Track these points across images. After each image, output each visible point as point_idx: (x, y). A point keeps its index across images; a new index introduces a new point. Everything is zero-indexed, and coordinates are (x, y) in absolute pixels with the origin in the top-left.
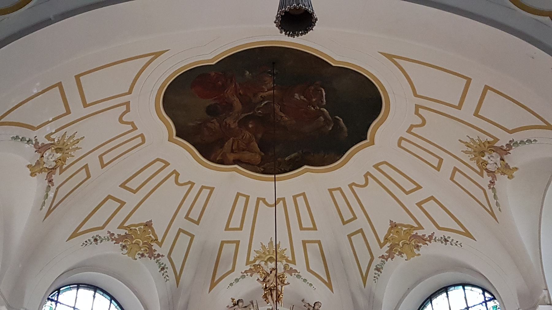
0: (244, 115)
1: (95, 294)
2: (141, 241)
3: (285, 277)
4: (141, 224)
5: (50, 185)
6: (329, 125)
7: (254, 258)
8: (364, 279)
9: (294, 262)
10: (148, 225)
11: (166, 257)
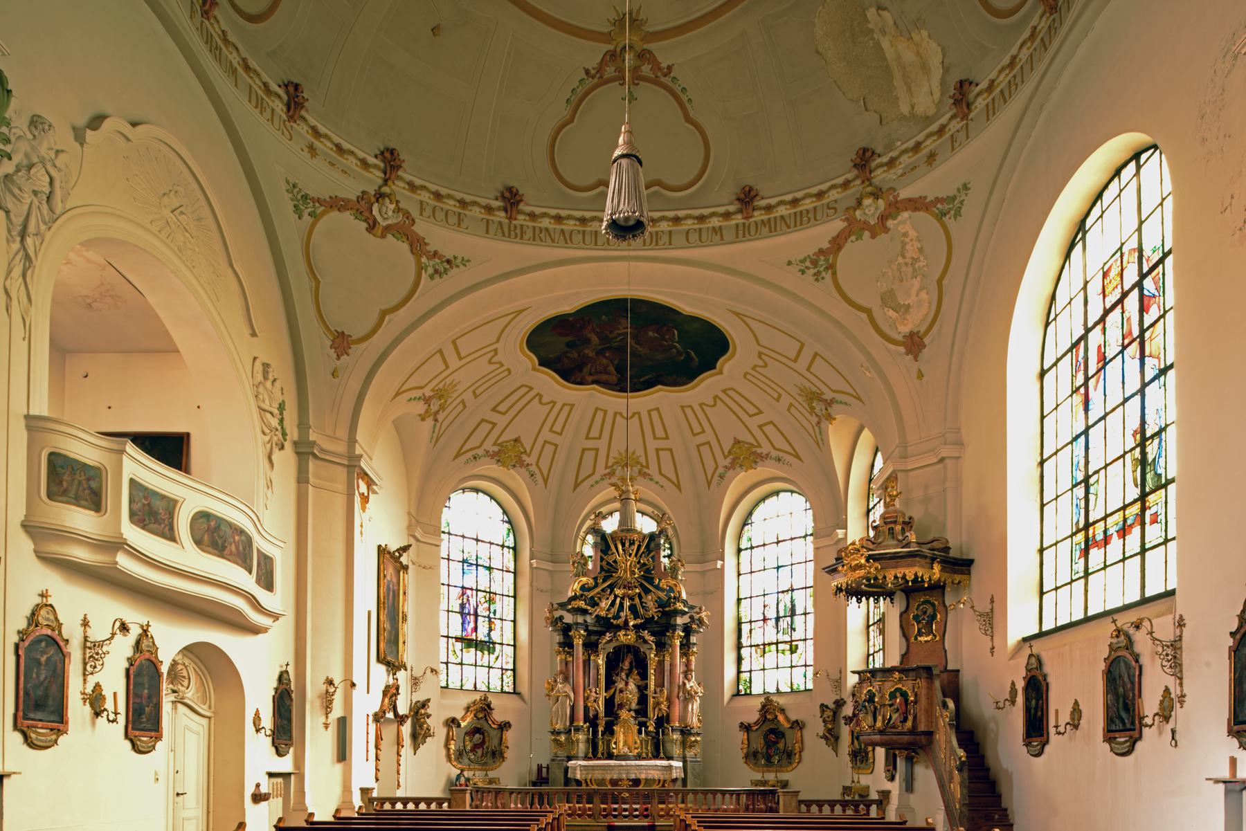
0: (601, 347)
4: (511, 440)
6: (681, 356)
8: (709, 483)
9: (647, 467)
10: (517, 440)
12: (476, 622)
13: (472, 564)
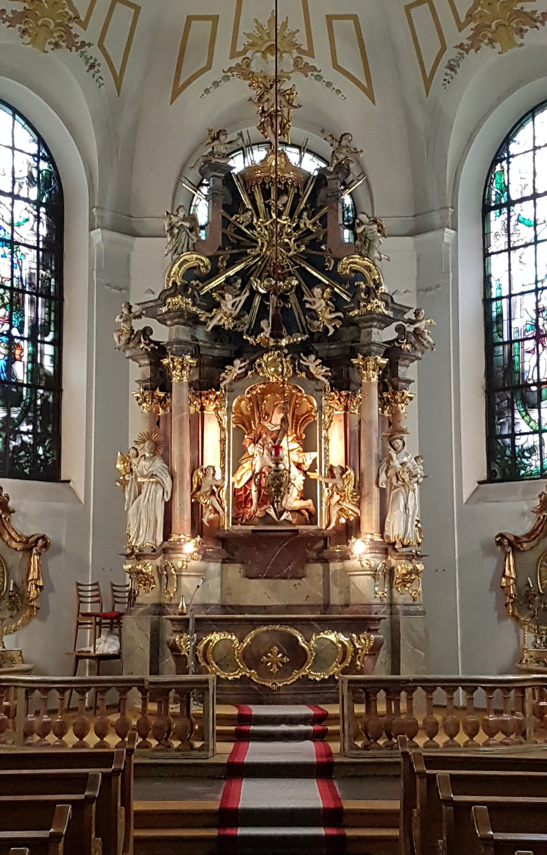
2: (50, 20)
3: (295, 93)
7: (243, 47)
8: (428, 82)
11: (96, 46)
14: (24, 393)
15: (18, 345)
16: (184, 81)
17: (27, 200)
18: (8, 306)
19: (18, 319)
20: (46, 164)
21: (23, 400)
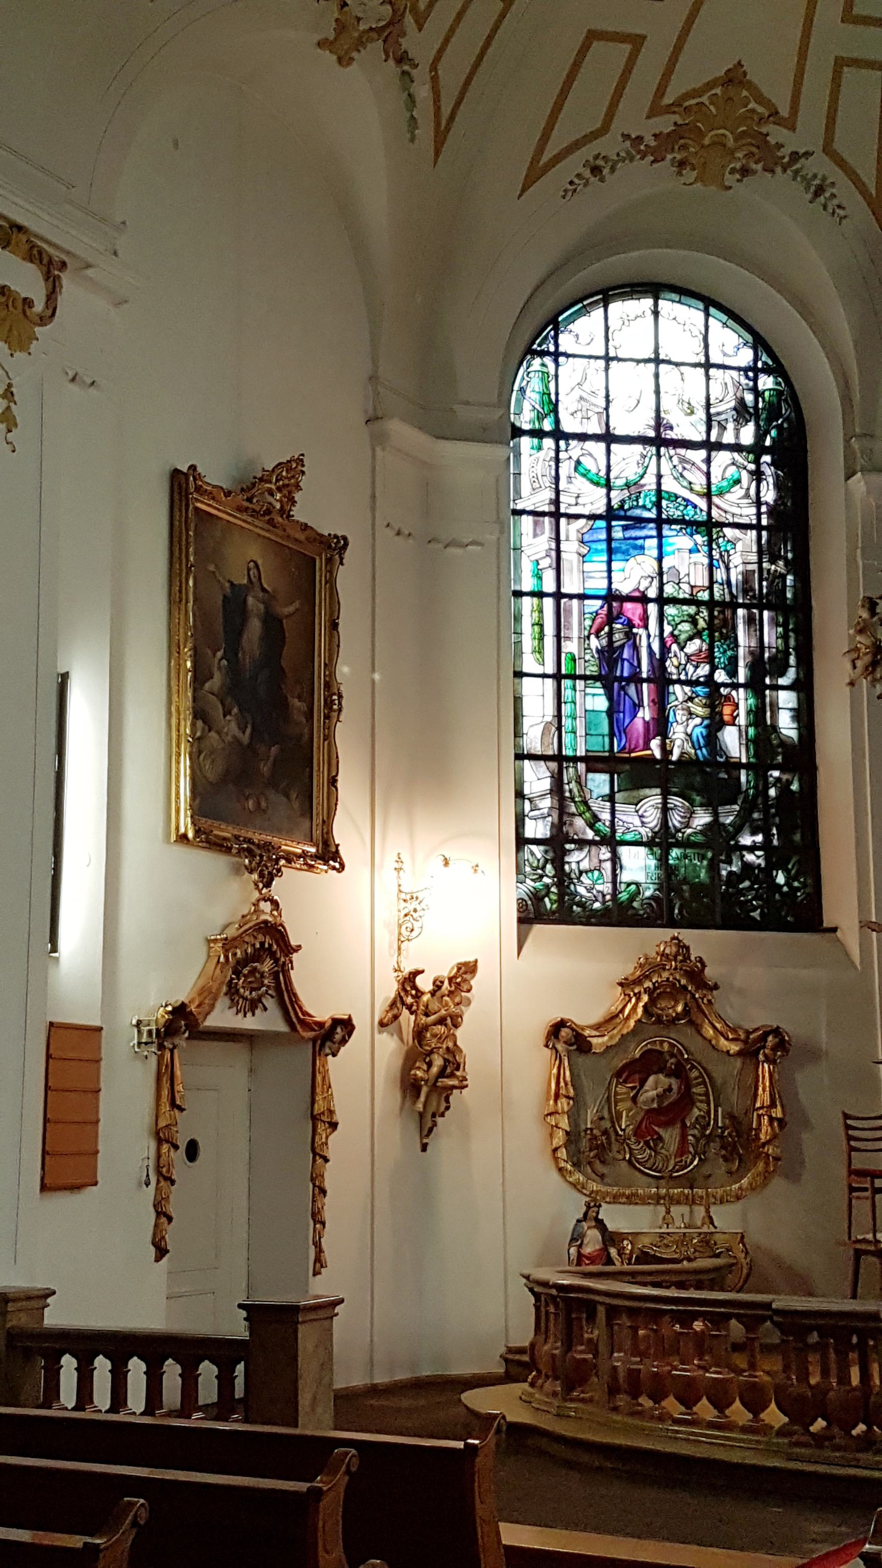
1: (656, 305)
2: (727, 133)
4: (710, 85)
5: (406, 68)
12: (661, 703)
13: (640, 522)
14: (743, 779)
15: (728, 698)
16: (551, 156)
17: (737, 448)
18: (706, 632)
19: (725, 652)
20: (771, 379)
21: (741, 793)
